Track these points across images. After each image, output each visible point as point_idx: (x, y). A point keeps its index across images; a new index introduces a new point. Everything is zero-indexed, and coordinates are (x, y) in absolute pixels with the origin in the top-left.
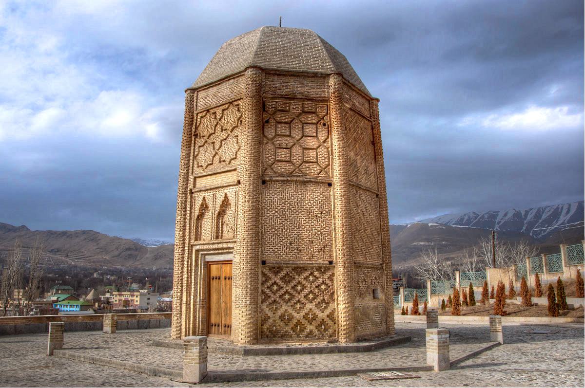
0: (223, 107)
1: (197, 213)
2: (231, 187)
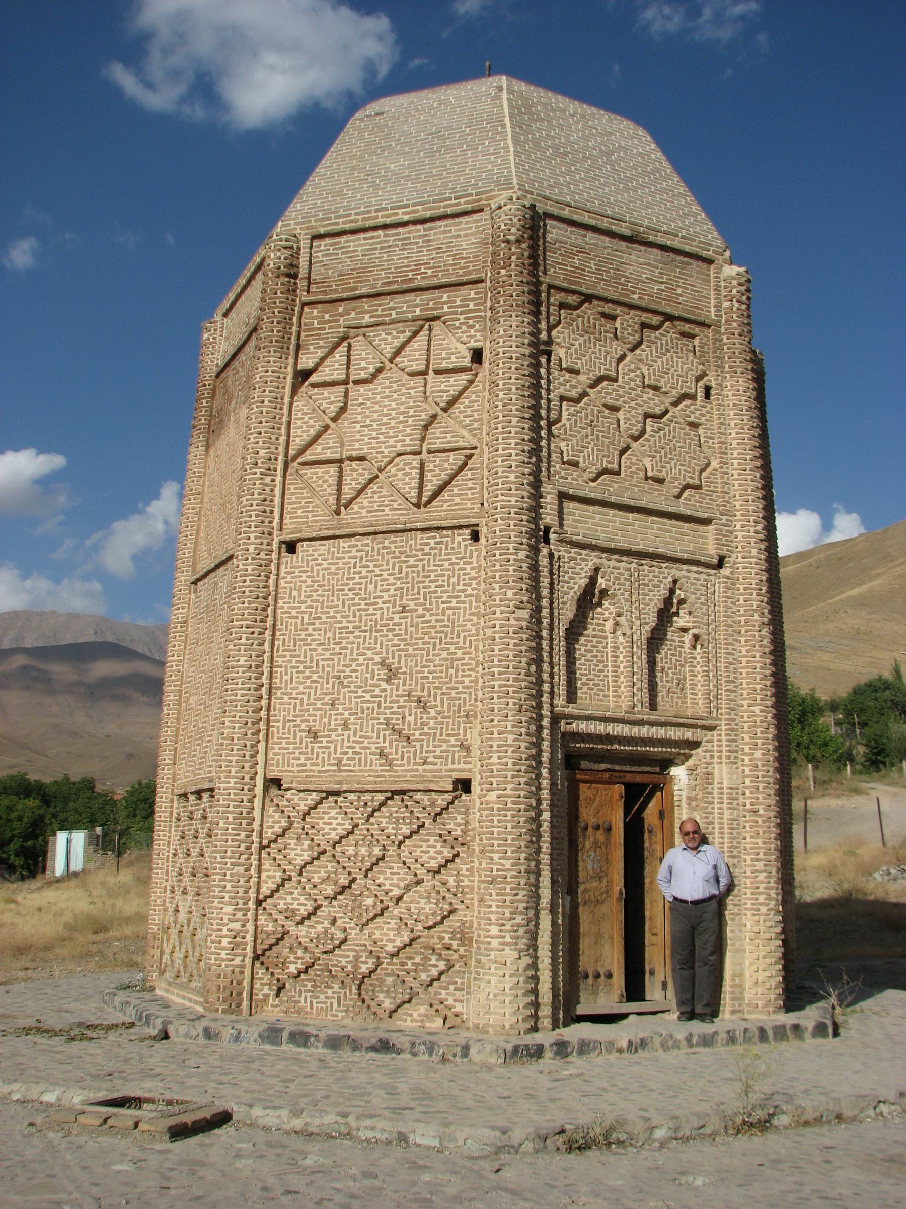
1: (568, 612)
2: (694, 568)
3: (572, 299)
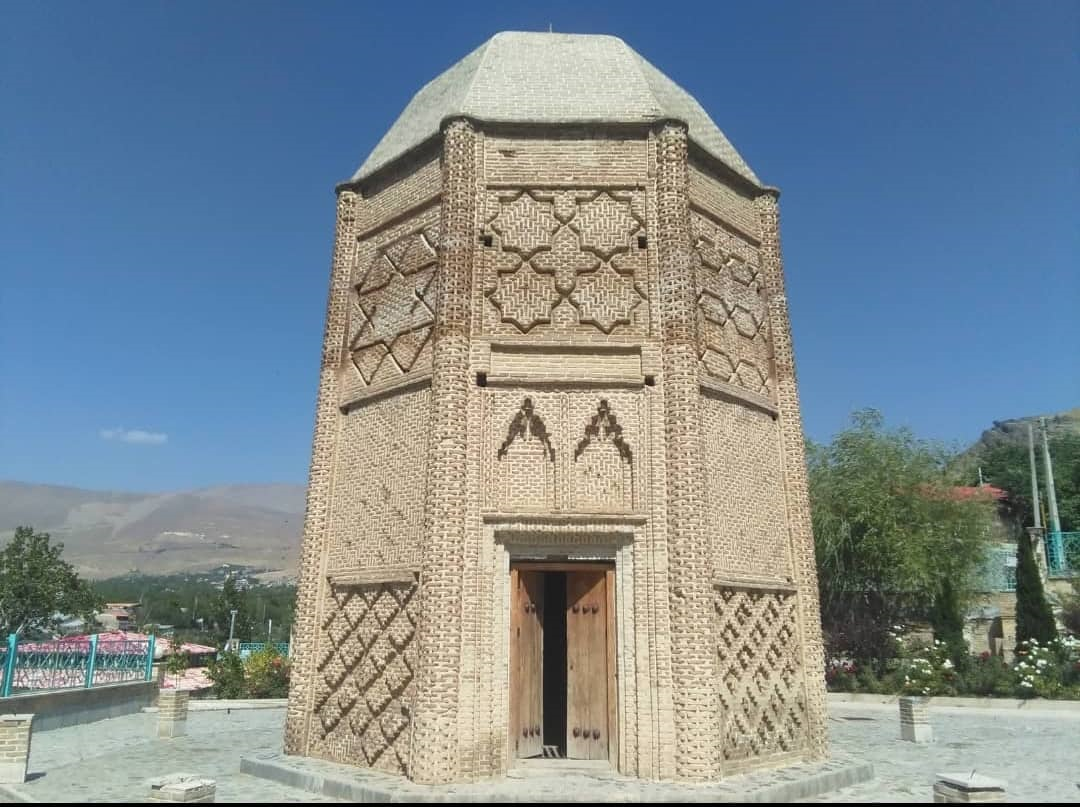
0: (577, 194)
3: (509, 193)
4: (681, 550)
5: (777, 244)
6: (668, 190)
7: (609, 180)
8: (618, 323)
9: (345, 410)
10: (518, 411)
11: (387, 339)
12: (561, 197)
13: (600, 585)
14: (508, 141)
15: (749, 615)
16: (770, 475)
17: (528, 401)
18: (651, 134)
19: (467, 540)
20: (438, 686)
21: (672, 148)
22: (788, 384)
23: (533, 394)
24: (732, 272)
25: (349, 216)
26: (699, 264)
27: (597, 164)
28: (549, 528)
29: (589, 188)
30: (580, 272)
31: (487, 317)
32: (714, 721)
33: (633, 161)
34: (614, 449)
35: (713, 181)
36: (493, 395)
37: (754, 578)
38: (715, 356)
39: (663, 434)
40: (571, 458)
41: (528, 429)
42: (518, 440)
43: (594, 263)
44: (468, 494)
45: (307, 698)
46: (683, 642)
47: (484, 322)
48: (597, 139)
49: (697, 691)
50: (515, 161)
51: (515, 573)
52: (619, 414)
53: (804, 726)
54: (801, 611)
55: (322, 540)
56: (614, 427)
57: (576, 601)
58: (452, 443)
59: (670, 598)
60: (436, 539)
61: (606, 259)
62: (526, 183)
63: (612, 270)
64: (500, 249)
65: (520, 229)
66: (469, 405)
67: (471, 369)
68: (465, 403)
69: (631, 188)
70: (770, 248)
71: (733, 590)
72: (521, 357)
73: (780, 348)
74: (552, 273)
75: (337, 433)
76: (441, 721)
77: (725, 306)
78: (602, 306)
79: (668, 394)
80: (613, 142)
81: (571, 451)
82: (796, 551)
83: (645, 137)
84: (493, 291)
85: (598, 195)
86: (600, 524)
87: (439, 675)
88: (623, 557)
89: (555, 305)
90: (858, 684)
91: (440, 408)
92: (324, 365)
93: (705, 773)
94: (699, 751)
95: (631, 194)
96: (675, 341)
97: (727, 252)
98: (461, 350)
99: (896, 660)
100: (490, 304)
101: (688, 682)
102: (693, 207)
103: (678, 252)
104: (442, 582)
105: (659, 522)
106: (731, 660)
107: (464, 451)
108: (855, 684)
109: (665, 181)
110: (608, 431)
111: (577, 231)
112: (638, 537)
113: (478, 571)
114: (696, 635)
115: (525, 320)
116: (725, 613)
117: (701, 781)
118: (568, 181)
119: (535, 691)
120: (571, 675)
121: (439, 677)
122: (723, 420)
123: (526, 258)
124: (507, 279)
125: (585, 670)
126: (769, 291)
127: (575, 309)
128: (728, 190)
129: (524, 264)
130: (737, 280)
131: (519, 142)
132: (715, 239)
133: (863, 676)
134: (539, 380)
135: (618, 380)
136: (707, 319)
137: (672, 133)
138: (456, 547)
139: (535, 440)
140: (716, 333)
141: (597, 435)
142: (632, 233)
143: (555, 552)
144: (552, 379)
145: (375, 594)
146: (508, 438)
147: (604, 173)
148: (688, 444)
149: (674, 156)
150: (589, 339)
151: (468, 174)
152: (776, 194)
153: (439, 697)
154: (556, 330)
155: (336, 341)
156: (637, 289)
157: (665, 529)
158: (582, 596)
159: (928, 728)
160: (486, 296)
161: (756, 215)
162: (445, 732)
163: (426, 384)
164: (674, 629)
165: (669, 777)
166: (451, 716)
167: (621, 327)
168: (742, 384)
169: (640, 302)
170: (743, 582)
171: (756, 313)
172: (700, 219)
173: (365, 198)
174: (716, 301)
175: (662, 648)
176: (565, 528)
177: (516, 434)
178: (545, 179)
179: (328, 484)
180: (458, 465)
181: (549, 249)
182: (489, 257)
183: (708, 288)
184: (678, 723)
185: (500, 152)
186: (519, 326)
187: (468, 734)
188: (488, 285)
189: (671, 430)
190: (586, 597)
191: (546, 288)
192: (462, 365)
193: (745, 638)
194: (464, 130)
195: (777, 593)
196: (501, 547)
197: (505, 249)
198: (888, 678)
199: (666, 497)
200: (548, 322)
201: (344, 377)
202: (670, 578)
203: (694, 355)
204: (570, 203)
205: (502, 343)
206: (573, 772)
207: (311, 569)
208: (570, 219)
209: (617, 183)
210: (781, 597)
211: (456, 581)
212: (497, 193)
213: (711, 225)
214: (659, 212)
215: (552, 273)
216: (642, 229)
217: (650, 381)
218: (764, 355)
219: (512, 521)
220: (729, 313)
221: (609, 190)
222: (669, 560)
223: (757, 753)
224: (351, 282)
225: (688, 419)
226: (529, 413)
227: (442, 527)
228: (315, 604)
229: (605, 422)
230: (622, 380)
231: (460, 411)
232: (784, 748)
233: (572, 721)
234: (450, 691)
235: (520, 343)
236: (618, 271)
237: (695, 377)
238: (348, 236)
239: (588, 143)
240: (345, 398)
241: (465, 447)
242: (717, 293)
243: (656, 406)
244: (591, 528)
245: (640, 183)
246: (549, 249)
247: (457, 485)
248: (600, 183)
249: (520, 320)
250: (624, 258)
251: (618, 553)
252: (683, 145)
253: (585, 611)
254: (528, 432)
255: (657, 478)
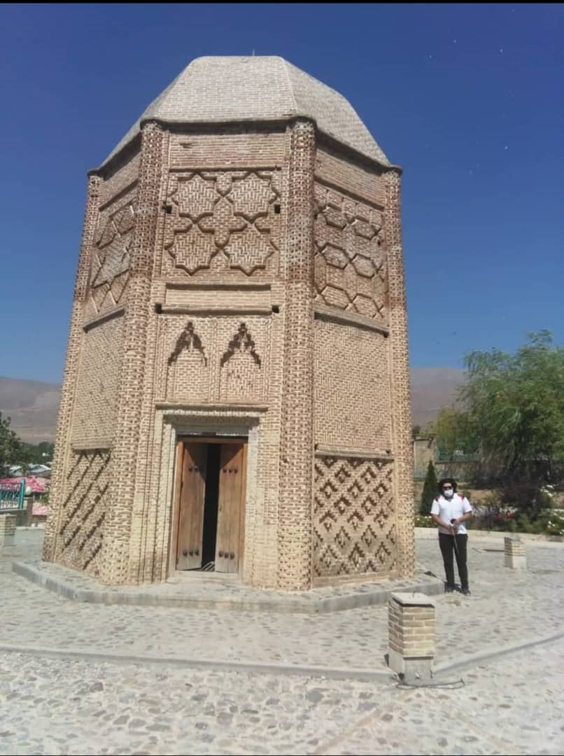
0: (233, 174)
3: (185, 175)
4: (288, 430)
5: (397, 209)
6: (297, 169)
7: (256, 164)
8: (256, 268)
9: (87, 329)
10: (183, 331)
11: (109, 280)
12: (222, 176)
13: (239, 454)
14: (187, 137)
15: (349, 476)
16: (378, 377)
17: (190, 324)
18: (288, 128)
19: (143, 420)
20: (116, 519)
21: (301, 138)
22: (398, 311)
23: (194, 319)
24: (355, 230)
25: (95, 193)
26: (324, 224)
27: (247, 152)
28: (201, 413)
29: (241, 170)
30: (232, 231)
31: (165, 265)
32: (304, 549)
33: (275, 148)
34: (250, 358)
35: (343, 162)
36: (166, 320)
37: (355, 450)
38: (333, 291)
39: (283, 347)
40: (218, 365)
41: (192, 344)
42: (184, 352)
43: (242, 224)
44: (145, 388)
45: (56, 524)
46: (286, 494)
47: (163, 268)
48: (250, 133)
49: (293, 529)
50: (191, 151)
51: (181, 444)
52: (253, 333)
53: (394, 555)
54: (396, 474)
55: (69, 419)
56: (250, 343)
57: (225, 465)
58: (134, 354)
59: (280, 464)
60: (120, 419)
61: (252, 221)
62: (197, 167)
63: (255, 229)
64: (178, 215)
65: (191, 201)
66: (149, 326)
67: (151, 301)
68: (146, 325)
69: (271, 169)
70: (391, 211)
71: (335, 459)
72: (188, 292)
73: (393, 284)
74: (212, 232)
75: (83, 346)
76: (117, 543)
77: (346, 255)
78: (246, 256)
79: (287, 319)
80: (260, 135)
81: (218, 360)
82: (396, 431)
83: (284, 131)
84: (170, 245)
85: (248, 174)
86: (236, 411)
87: (117, 512)
88: (253, 434)
89: (213, 255)
90: (516, 526)
91: (127, 329)
92: (75, 298)
93: (295, 584)
94: (292, 570)
95: (271, 173)
96: (294, 281)
97: (351, 215)
98: (143, 287)
99: (548, 510)
100: (168, 255)
101: (287, 522)
102: (317, 179)
103: (300, 215)
104: (123, 449)
105: (276, 410)
106: (329, 506)
107: (143, 359)
108: (514, 526)
109: (295, 163)
110: (247, 345)
111: (231, 201)
112: (263, 420)
113: (150, 443)
114: (294, 489)
115: (191, 266)
116: (326, 474)
117: (292, 590)
118: (228, 165)
119: (196, 525)
120: (220, 514)
121: (117, 513)
122: (332, 339)
123: (195, 222)
124: (181, 237)
125: (228, 511)
126: (388, 243)
127: (227, 258)
128: (357, 169)
129: (194, 226)
130: (360, 235)
131: (195, 137)
132: (342, 205)
133: (520, 521)
134: (197, 309)
135: (253, 309)
136: (328, 264)
137: (302, 127)
138: (133, 426)
139: (197, 351)
140: (336, 275)
141: (239, 348)
142: (270, 202)
143: (207, 430)
144: (206, 308)
145: (92, 456)
146: (176, 349)
147: (253, 158)
148: (298, 355)
149: (302, 144)
150: (234, 280)
151: (156, 160)
152: (399, 172)
153: (117, 528)
154: (212, 273)
155: (83, 283)
156: (272, 243)
157: (280, 415)
158: (228, 461)
159: (523, 559)
160: (166, 249)
161: (384, 188)
162: (120, 550)
163: (120, 313)
164: (280, 485)
165: (272, 587)
166: (124, 540)
167: (259, 271)
168: (358, 311)
169: (273, 253)
170: (343, 452)
171: (375, 260)
172: (328, 191)
173: (105, 180)
174: (338, 251)
175: (273, 497)
176: (211, 414)
177: (183, 347)
178: (211, 164)
179: (73, 380)
180: (138, 368)
181: (211, 215)
182: (169, 221)
183: (331, 242)
184: (279, 550)
185: (181, 144)
186: (187, 271)
187: (136, 553)
188: (167, 241)
189: (288, 345)
190: (231, 462)
191: (208, 245)
192: (144, 298)
193: (343, 491)
194: (154, 129)
195: (376, 461)
196: (169, 426)
197: (182, 215)
198: (538, 523)
199: (281, 392)
200: (208, 268)
201: (87, 306)
202: (280, 450)
203: (308, 290)
204: (228, 181)
205: (174, 283)
206: (212, 581)
207: (61, 438)
208: (228, 192)
209: (262, 166)
210: (380, 464)
211: (132, 449)
212: (177, 175)
213: (339, 196)
214: (290, 185)
215: (212, 232)
216: (279, 199)
217: (276, 309)
218: (381, 289)
219: (175, 408)
220: (351, 260)
221: (256, 171)
222: (281, 437)
223: (347, 572)
224: (94, 240)
225: (299, 336)
226: (191, 332)
227: (124, 411)
228: (64, 460)
229: (242, 339)
230: (257, 309)
231: (141, 331)
232: (374, 570)
233: (219, 547)
234: (125, 524)
235: (186, 283)
236: (260, 230)
237: (307, 307)
238: (94, 207)
239: (243, 136)
240: (87, 321)
241: (144, 356)
242: (340, 245)
243: (279, 328)
244: (229, 413)
245: (278, 165)
246: (211, 215)
247: (136, 382)
248: (249, 166)
249: (187, 267)
250: (264, 221)
251: (250, 431)
252: (310, 136)
253: (230, 471)
254: (191, 346)
255: (277, 378)
